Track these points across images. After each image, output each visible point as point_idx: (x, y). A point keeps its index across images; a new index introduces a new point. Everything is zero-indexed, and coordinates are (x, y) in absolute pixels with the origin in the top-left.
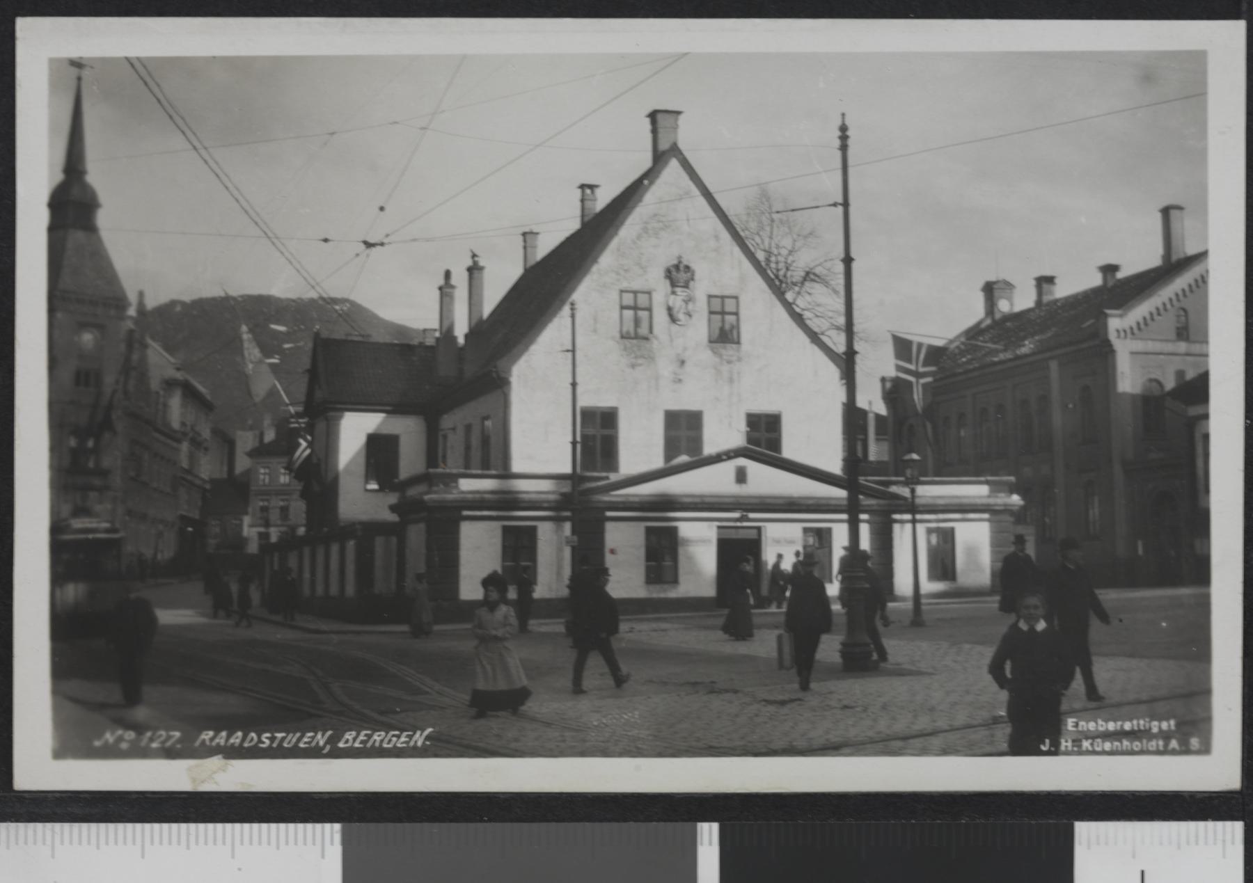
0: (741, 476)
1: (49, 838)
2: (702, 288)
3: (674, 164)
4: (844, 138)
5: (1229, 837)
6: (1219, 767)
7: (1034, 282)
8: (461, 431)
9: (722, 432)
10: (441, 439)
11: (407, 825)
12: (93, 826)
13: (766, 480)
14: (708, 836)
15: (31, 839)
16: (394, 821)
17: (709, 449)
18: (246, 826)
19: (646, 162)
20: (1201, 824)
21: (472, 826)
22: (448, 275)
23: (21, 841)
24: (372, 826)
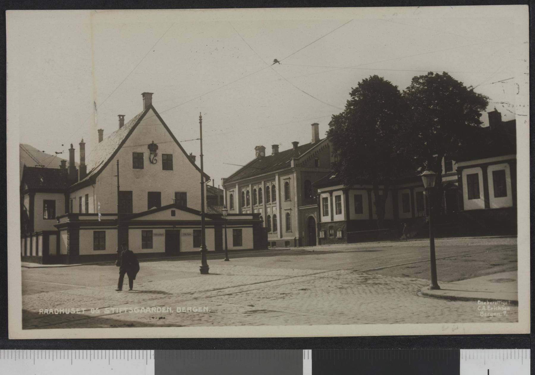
0: (173, 214)
1: (32, 356)
2: (160, 152)
3: (151, 110)
4: (201, 120)
5: (524, 356)
6: (523, 326)
7: (132, 154)
8: (78, 199)
9: (167, 199)
10: (70, 201)
11: (182, 351)
12: (51, 351)
13: (181, 215)
14: (307, 355)
15: (25, 357)
16: (176, 349)
17: (162, 205)
18: (115, 351)
19: (141, 109)
20: (513, 350)
21: (209, 351)
22: (72, 145)
23: (21, 357)
24: (167, 351)
